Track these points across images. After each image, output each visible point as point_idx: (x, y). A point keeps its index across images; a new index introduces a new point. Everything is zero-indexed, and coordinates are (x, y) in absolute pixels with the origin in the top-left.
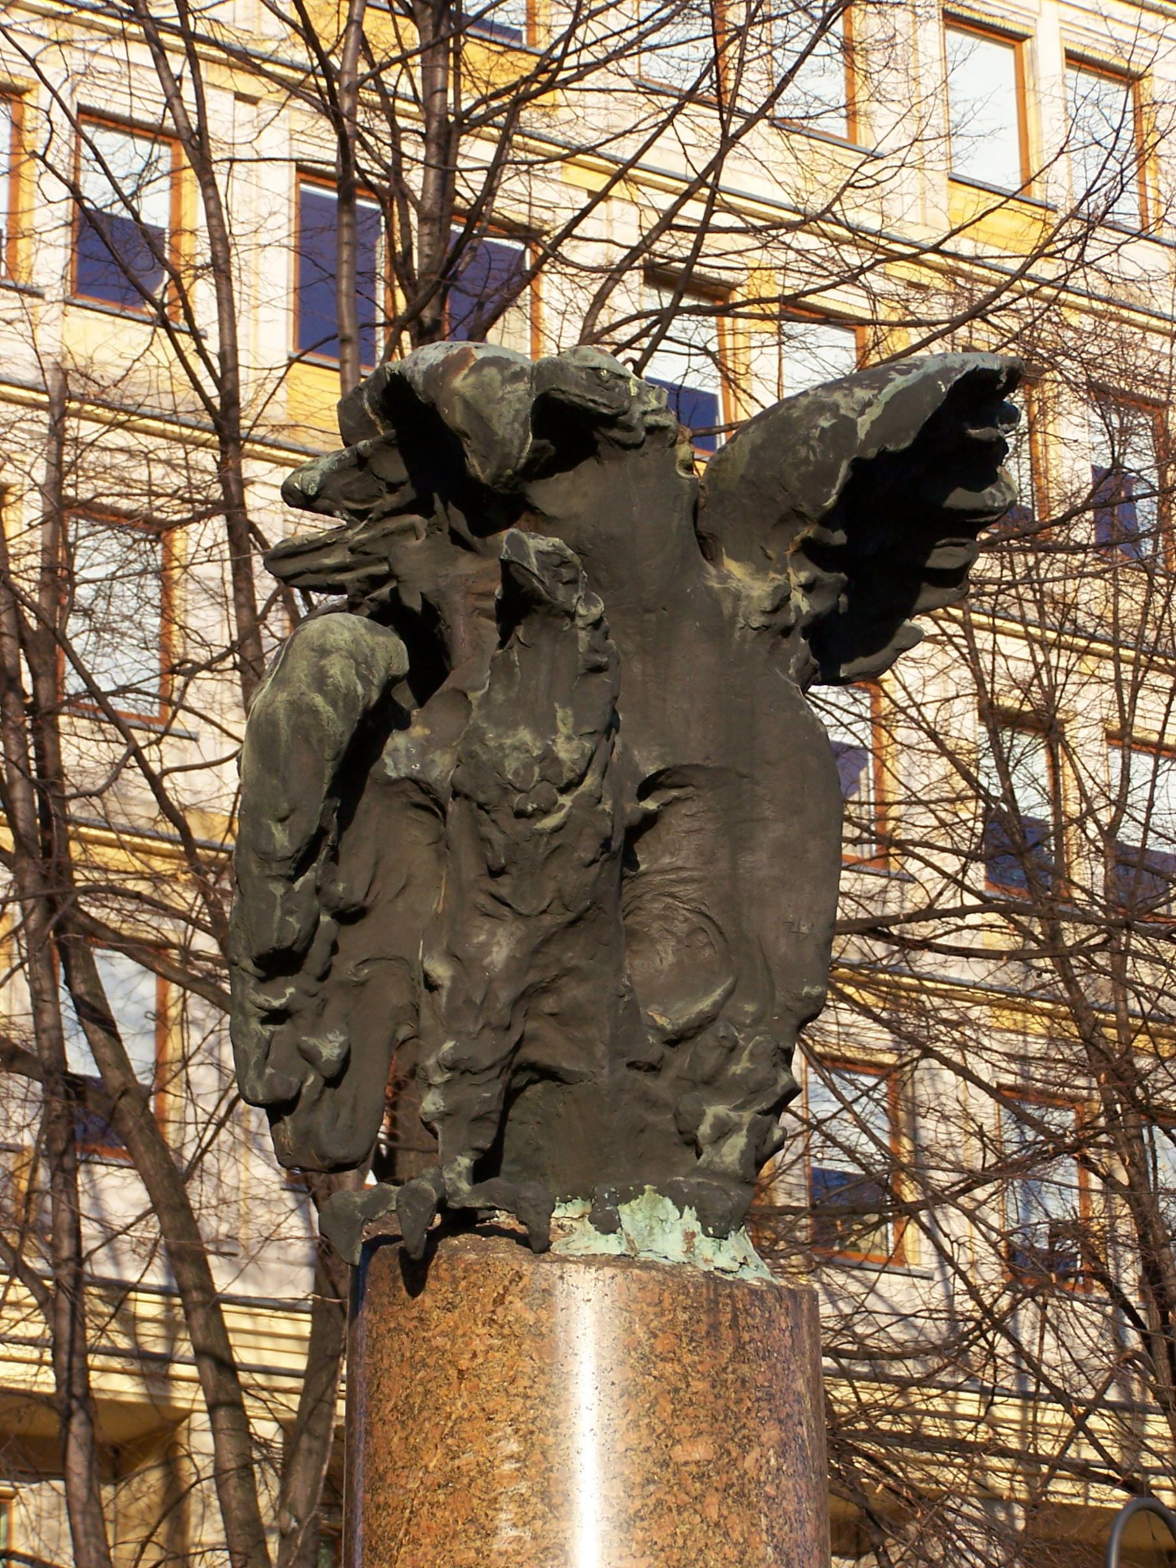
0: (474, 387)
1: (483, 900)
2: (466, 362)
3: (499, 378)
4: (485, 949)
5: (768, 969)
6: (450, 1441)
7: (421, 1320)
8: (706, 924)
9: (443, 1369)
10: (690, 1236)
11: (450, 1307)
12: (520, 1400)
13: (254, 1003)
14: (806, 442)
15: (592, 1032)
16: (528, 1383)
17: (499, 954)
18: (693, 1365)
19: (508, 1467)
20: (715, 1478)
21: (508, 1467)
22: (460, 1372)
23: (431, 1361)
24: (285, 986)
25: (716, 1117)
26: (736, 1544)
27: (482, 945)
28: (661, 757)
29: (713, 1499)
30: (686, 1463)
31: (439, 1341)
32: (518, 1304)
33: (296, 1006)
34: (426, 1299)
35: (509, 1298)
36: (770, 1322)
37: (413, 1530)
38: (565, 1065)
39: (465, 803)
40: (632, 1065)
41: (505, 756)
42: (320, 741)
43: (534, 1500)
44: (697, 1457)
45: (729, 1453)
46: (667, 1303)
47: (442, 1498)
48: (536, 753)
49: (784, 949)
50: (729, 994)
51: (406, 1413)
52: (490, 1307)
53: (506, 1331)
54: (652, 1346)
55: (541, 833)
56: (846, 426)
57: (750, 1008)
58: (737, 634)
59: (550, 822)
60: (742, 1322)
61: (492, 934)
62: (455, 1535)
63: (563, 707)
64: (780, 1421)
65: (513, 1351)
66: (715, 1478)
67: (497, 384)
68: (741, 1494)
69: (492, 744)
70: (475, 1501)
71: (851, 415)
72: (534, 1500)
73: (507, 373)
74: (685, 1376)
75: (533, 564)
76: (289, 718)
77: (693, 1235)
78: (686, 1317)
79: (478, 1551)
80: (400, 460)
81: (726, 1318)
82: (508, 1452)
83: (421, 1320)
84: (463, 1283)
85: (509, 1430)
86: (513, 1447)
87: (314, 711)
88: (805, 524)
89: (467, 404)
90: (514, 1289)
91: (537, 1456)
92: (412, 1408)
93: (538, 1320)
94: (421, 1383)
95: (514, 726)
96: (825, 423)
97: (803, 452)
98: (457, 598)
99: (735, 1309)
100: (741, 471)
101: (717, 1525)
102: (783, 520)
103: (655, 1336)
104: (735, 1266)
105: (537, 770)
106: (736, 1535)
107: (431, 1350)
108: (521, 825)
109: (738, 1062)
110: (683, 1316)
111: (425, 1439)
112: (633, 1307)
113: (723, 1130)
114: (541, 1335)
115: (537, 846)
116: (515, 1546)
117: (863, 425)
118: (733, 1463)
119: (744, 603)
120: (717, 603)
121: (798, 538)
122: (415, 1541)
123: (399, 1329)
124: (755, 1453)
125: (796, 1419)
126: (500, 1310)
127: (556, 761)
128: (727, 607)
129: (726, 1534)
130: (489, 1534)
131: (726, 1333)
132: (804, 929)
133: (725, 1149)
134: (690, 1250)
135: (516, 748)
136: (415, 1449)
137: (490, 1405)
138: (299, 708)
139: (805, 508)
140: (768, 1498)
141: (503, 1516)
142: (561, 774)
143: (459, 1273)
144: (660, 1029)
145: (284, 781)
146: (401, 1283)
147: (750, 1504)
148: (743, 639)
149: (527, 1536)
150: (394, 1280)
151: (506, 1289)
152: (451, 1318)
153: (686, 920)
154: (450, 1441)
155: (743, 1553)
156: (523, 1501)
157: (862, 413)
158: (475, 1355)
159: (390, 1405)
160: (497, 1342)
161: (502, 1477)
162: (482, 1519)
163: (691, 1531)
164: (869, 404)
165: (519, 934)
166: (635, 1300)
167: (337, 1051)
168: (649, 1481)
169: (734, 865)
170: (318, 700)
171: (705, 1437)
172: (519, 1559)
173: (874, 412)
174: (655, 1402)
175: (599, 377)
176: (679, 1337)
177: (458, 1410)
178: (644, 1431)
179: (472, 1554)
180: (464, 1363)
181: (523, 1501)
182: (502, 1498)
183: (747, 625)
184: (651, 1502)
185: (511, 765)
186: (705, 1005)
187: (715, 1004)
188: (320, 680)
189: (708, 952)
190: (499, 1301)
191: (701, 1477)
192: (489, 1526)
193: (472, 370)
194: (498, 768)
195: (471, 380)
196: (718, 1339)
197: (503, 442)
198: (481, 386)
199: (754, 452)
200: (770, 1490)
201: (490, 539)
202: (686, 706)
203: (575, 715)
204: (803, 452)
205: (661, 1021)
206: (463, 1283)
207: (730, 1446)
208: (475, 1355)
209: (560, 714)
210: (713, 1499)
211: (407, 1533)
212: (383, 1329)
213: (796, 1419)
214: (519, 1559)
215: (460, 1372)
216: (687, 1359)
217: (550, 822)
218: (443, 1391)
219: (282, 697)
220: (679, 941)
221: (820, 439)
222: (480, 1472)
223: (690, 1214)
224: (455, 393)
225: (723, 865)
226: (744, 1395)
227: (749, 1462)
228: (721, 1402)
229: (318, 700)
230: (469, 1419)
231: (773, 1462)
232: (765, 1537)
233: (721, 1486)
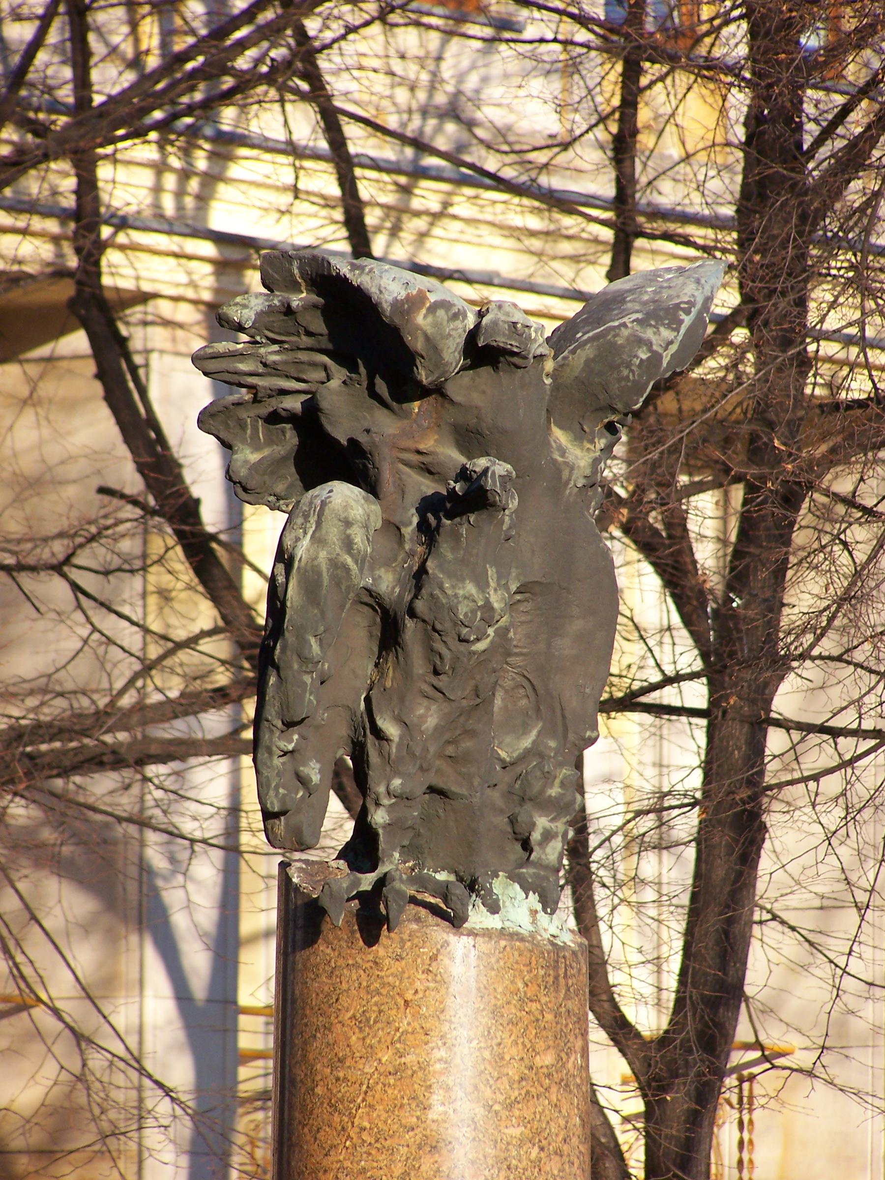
1: (426, 688)
2: (424, 304)
3: (446, 318)
4: (422, 718)
5: (564, 717)
6: (398, 1045)
7: (376, 963)
8: (525, 683)
9: (393, 998)
10: (534, 913)
11: (399, 958)
13: (278, 748)
14: (628, 365)
15: (473, 770)
17: (431, 722)
18: (546, 1004)
24: (292, 735)
25: (545, 829)
27: (421, 717)
29: (554, 1089)
34: (379, 950)
37: (369, 1099)
38: (453, 789)
39: (420, 624)
42: (348, 587)
44: (547, 1063)
48: (480, 603)
49: (575, 703)
51: (362, 1022)
52: (428, 962)
54: (525, 993)
55: (474, 653)
56: (656, 358)
58: (568, 492)
59: (481, 646)
61: (428, 709)
62: (402, 1106)
66: (555, 1076)
67: (445, 323)
68: (567, 1085)
69: (449, 592)
70: (416, 1086)
71: (660, 350)
73: (450, 313)
74: (542, 1011)
76: (328, 570)
77: (536, 912)
79: (418, 1118)
80: (321, 319)
81: (561, 972)
83: (376, 963)
84: (409, 944)
88: (614, 413)
89: (427, 338)
92: (368, 1020)
94: (376, 1004)
95: (462, 580)
96: (644, 356)
97: (625, 372)
98: (386, 451)
100: (576, 374)
102: (601, 409)
105: (479, 614)
106: (564, 1112)
107: (383, 985)
108: (462, 647)
109: (552, 787)
110: (542, 972)
111: (379, 1042)
112: (515, 966)
113: (548, 836)
115: (469, 660)
116: (443, 1117)
118: (563, 1066)
119: (575, 472)
120: (559, 471)
121: (606, 421)
123: (356, 966)
126: (434, 964)
127: (492, 609)
128: (565, 474)
129: (560, 1111)
131: (562, 981)
132: (588, 691)
134: (534, 922)
137: (427, 1026)
138: (335, 564)
139: (619, 406)
143: (406, 937)
145: (323, 613)
146: (358, 935)
148: (570, 494)
150: (353, 932)
151: (438, 950)
152: (397, 967)
153: (513, 679)
154: (398, 1045)
157: (666, 349)
158: (416, 992)
159: (349, 1014)
160: (432, 985)
161: (435, 1072)
162: (422, 1098)
163: (544, 1110)
164: (671, 342)
165: (446, 711)
166: (517, 963)
169: (549, 645)
170: (349, 561)
173: (674, 348)
174: (526, 1028)
175: (515, 327)
176: (539, 986)
177: (404, 1026)
178: (520, 1047)
179: (414, 1120)
180: (409, 996)
182: (434, 1086)
184: (523, 1092)
185: (463, 610)
188: (348, 544)
189: (524, 702)
191: (549, 1076)
192: (426, 1103)
193: (429, 309)
194: (453, 610)
197: (448, 364)
198: (436, 325)
199: (588, 362)
201: (405, 405)
202: (532, 540)
204: (625, 372)
205: (503, 754)
206: (409, 944)
208: (416, 992)
210: (554, 1089)
211: (364, 1100)
212: (341, 962)
216: (544, 1000)
218: (394, 1012)
220: (506, 692)
221: (639, 366)
222: (420, 1068)
223: (534, 898)
224: (418, 328)
225: (542, 646)
229: (349, 561)
230: (413, 1033)
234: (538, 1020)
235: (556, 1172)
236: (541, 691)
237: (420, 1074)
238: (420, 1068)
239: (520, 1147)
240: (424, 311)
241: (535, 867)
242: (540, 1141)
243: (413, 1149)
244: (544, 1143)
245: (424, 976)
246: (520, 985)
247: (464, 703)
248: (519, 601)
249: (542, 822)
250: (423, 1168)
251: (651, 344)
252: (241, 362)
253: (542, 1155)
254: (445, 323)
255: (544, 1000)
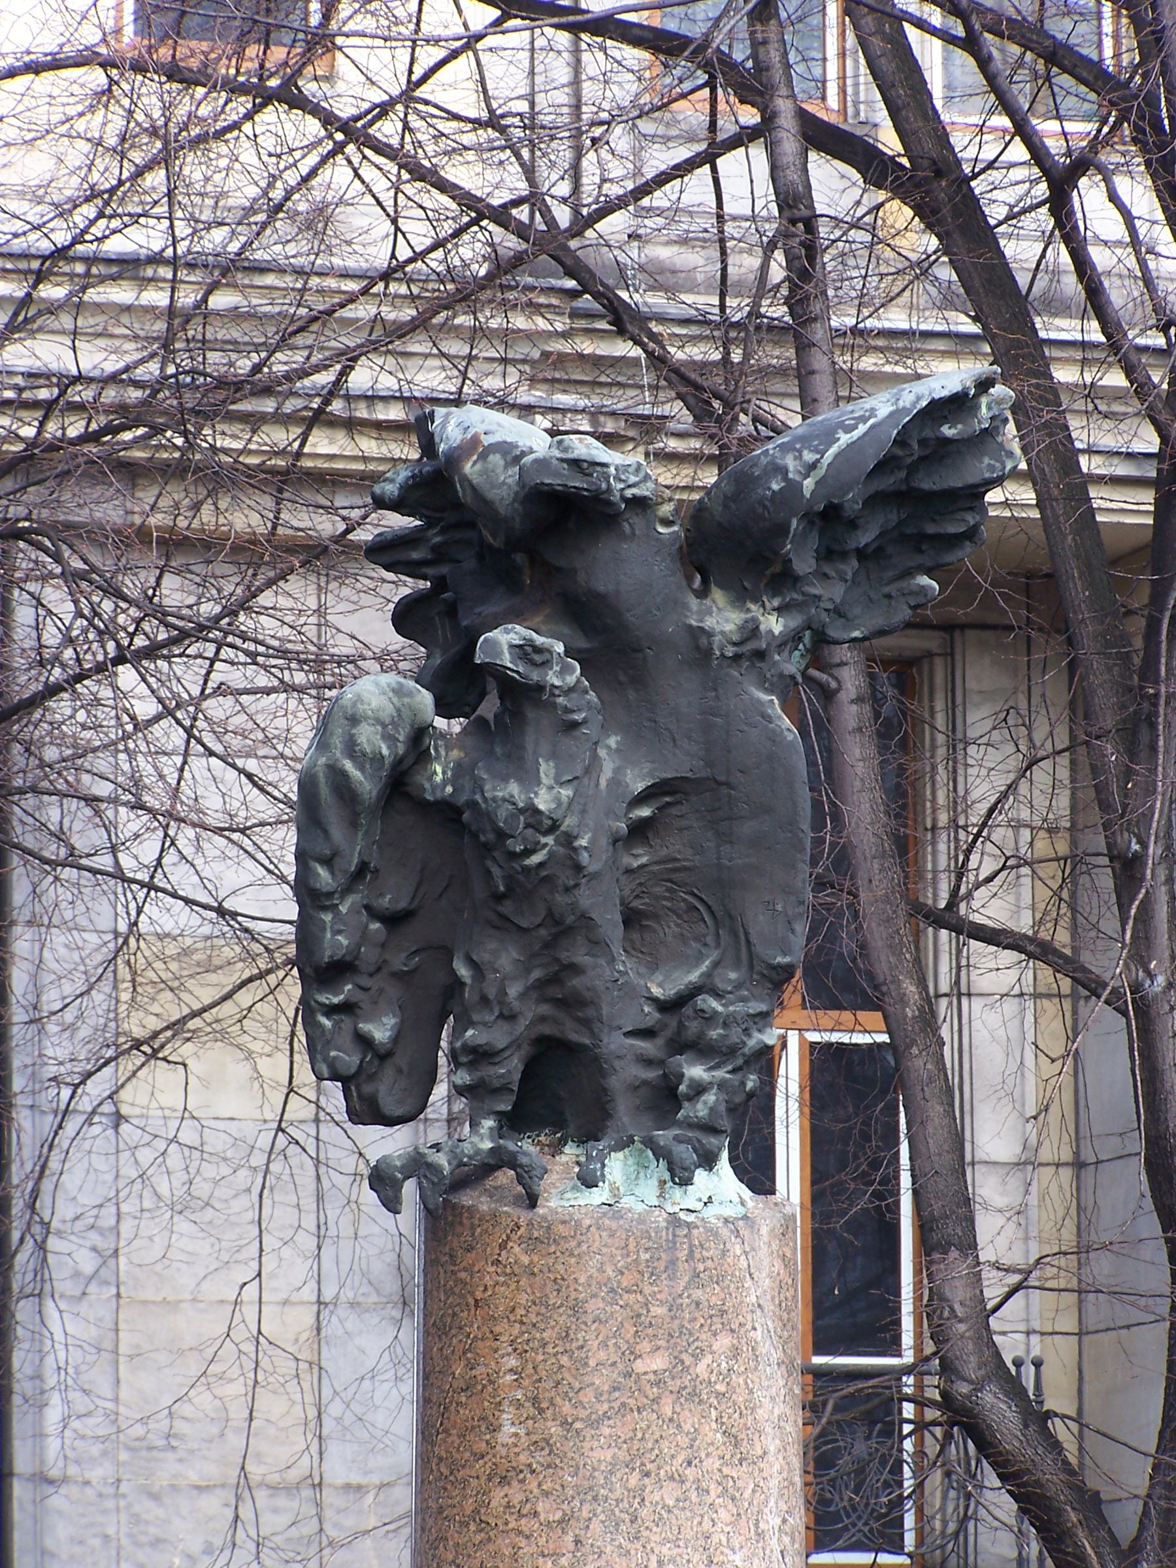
0: (482, 473)
3: (502, 463)
5: (748, 942)
12: (517, 1325)
16: (523, 1312)
19: (510, 1378)
20: (670, 1383)
21: (510, 1378)
22: (476, 1301)
23: (457, 1290)
26: (688, 1433)
28: (651, 774)
30: (645, 1373)
31: (463, 1275)
32: (517, 1249)
33: (354, 1000)
35: (510, 1244)
36: (724, 1252)
40: (628, 1034)
41: (498, 807)
43: (527, 1404)
45: (683, 1362)
46: (632, 1247)
47: (464, 1399)
50: (716, 965)
53: (508, 1270)
57: (733, 975)
59: (536, 859)
60: (697, 1256)
63: (547, 761)
64: (732, 1331)
65: (513, 1287)
66: (670, 1383)
68: (694, 1394)
71: (798, 478)
72: (527, 1404)
75: (507, 660)
78: (647, 1256)
79: (487, 1442)
81: (682, 1255)
82: (508, 1367)
85: (510, 1349)
86: (513, 1362)
87: (344, 774)
90: (514, 1237)
91: (529, 1369)
93: (531, 1262)
95: (505, 779)
99: (691, 1246)
101: (671, 1420)
103: (622, 1273)
104: (698, 1206)
106: (687, 1427)
110: (645, 1256)
114: (533, 1274)
117: (809, 484)
122: (446, 1431)
124: (708, 1359)
125: (749, 1326)
126: (504, 1253)
129: (679, 1426)
130: (495, 1429)
131: (682, 1266)
133: (700, 1106)
135: (504, 800)
136: (447, 1358)
137: (497, 1329)
140: (718, 1395)
141: (505, 1416)
142: (541, 822)
144: (654, 1000)
147: (701, 1402)
149: (522, 1432)
151: (508, 1237)
155: (694, 1440)
156: (519, 1405)
157: (807, 476)
158: (486, 1289)
160: (502, 1279)
167: (388, 1034)
168: (615, 1389)
170: (348, 765)
171: (662, 1351)
172: (516, 1450)
176: (641, 1273)
178: (612, 1349)
179: (484, 1445)
180: (479, 1295)
181: (519, 1405)
183: (722, 655)
184: (616, 1405)
185: (503, 813)
186: (694, 976)
187: (702, 975)
188: (351, 747)
190: (503, 1246)
192: (495, 1423)
195: (478, 466)
196: (675, 1272)
198: (484, 472)
200: (721, 1387)
203: (556, 767)
207: (684, 1356)
208: (486, 1289)
209: (543, 767)
213: (749, 1326)
214: (516, 1450)
215: (476, 1301)
217: (536, 859)
219: (322, 761)
222: (490, 1381)
226: (697, 1315)
227: (701, 1368)
228: (677, 1322)
229: (348, 765)
231: (724, 1365)
232: (714, 1426)
233: (675, 1389)
234: (639, 1316)
235: (671, 1503)
236: (719, 914)
237: (490, 1389)
238: (490, 1381)
239: (611, 1473)
240: (475, 457)
241: (680, 1128)
242: (643, 1464)
243: (483, 1479)
244: (649, 1466)
245: (492, 1269)
246: (610, 1272)
247: (543, 932)
248: (668, 803)
249: (696, 1071)
250: (493, 1504)
251: (787, 472)
252: (414, 549)
253: (646, 1481)
254: (500, 470)
255: (647, 1290)
